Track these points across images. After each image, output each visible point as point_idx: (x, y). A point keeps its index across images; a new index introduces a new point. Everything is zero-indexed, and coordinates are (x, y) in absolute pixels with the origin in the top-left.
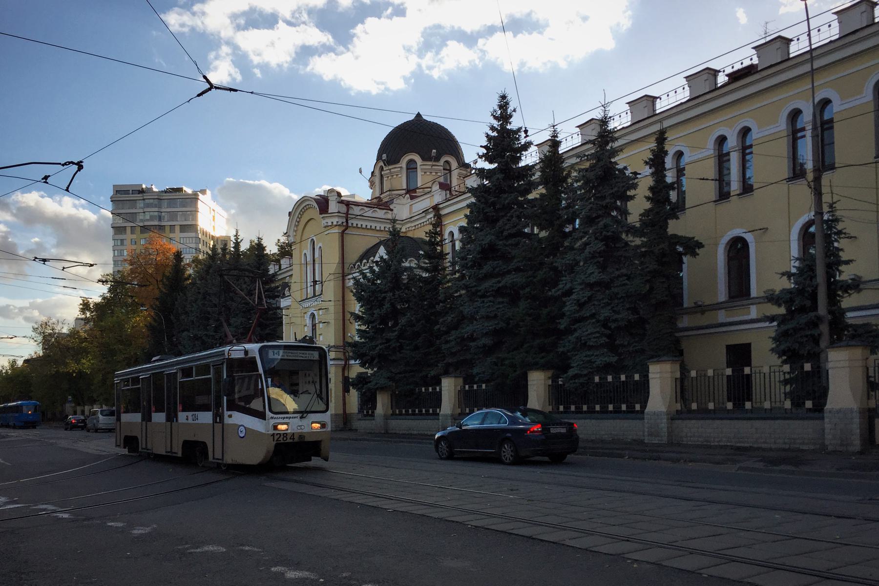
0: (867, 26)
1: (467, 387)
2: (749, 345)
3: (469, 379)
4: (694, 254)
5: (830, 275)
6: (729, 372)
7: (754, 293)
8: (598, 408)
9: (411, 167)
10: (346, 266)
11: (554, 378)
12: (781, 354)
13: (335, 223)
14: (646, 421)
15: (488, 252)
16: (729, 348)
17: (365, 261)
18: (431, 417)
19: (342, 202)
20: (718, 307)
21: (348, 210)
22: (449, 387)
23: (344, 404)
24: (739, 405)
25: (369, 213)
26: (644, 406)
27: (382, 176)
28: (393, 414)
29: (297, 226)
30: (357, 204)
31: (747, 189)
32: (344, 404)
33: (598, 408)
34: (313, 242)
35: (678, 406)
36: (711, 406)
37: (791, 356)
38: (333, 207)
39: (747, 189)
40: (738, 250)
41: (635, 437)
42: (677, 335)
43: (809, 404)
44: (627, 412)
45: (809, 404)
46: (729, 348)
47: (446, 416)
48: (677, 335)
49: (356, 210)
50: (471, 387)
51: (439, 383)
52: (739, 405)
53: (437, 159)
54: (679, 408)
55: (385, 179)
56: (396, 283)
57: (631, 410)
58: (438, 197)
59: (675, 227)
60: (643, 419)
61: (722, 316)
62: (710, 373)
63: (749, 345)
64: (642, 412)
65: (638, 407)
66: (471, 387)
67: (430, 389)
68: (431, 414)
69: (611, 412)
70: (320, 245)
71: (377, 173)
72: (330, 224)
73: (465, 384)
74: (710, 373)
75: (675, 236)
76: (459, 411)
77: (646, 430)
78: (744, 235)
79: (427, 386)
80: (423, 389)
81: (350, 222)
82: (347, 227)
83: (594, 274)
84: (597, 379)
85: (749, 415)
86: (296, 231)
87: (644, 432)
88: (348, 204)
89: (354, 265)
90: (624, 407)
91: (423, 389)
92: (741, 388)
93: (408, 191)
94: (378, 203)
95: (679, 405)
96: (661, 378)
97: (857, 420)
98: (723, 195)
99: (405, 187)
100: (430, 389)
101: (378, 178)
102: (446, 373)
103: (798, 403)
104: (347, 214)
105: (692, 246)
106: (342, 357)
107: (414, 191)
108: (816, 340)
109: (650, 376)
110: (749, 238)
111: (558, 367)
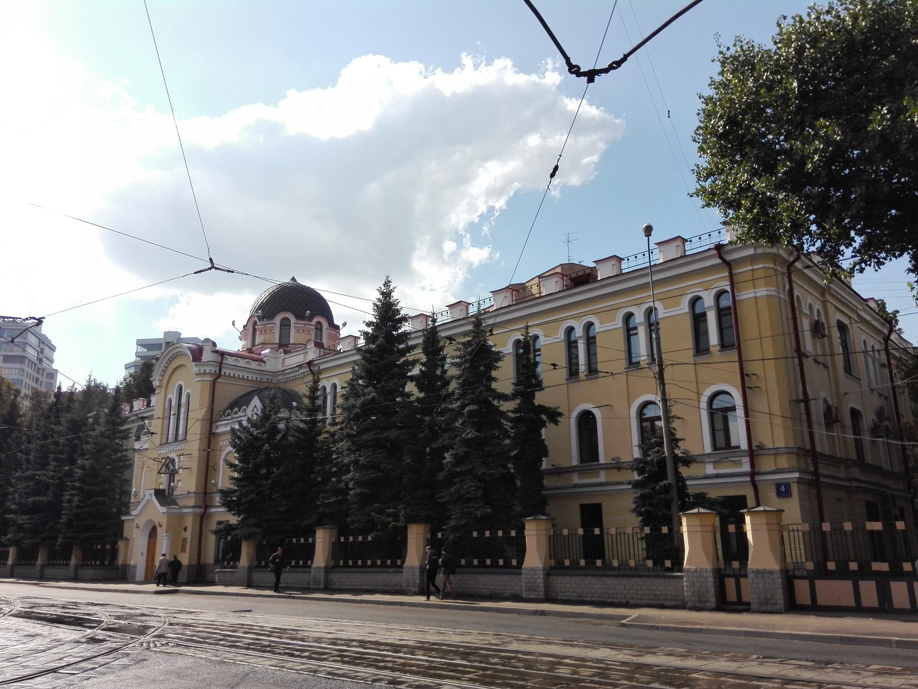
0: (616, 275)
1: (342, 539)
2: (600, 505)
3: (343, 530)
4: (556, 423)
5: (671, 450)
6: (581, 531)
7: (602, 460)
8: (476, 562)
9: (285, 324)
10: (214, 416)
11: (433, 533)
12: (640, 514)
13: (207, 371)
14: (523, 576)
15: (368, 409)
16: (583, 507)
17: (236, 409)
18: (302, 570)
19: (216, 352)
20: (570, 470)
21: (222, 359)
22: (322, 540)
23: (199, 555)
24: (590, 564)
25: (242, 363)
26: (403, 562)
27: (254, 330)
28: (336, 566)
29: (162, 376)
30: (231, 355)
31: (592, 371)
32: (199, 555)
33: (476, 562)
34: (181, 388)
35: (553, 563)
36: (632, 563)
37: (648, 518)
38: (207, 356)
39: (592, 371)
40: (587, 421)
41: (513, 592)
42: (544, 493)
43: (668, 563)
44: (585, 568)
45: (668, 563)
46: (583, 507)
47: (318, 568)
48: (544, 493)
49: (230, 361)
50: (347, 539)
51: (313, 534)
52: (590, 564)
53: (310, 319)
54: (553, 564)
55: (258, 333)
56: (274, 430)
57: (394, 565)
58: (312, 353)
59: (540, 399)
60: (521, 574)
61: (576, 479)
62: (565, 532)
63: (600, 505)
64: (401, 566)
65: (514, 562)
66: (347, 539)
67: (302, 540)
68: (301, 567)
69: (476, 567)
70: (189, 390)
71: (250, 327)
72: (202, 371)
73: (340, 535)
74: (565, 532)
75: (541, 406)
76: (333, 563)
77: (524, 585)
78: (594, 410)
79: (298, 536)
80: (294, 540)
81: (223, 371)
82: (219, 376)
83: (470, 433)
84: (475, 534)
85: (633, 572)
86: (162, 376)
87: (521, 587)
88: (222, 354)
89: (224, 413)
90: (501, 562)
91: (294, 540)
92: (594, 548)
93: (281, 345)
94: (251, 353)
95: (553, 561)
96: (535, 536)
97: (711, 579)
98: (573, 373)
99: (277, 341)
100: (302, 540)
101: (251, 329)
102: (320, 524)
103: (658, 562)
104: (221, 363)
105: (554, 415)
106: (202, 505)
107: (287, 346)
108: (668, 504)
109: (526, 533)
110: (597, 413)
111: (436, 522)
